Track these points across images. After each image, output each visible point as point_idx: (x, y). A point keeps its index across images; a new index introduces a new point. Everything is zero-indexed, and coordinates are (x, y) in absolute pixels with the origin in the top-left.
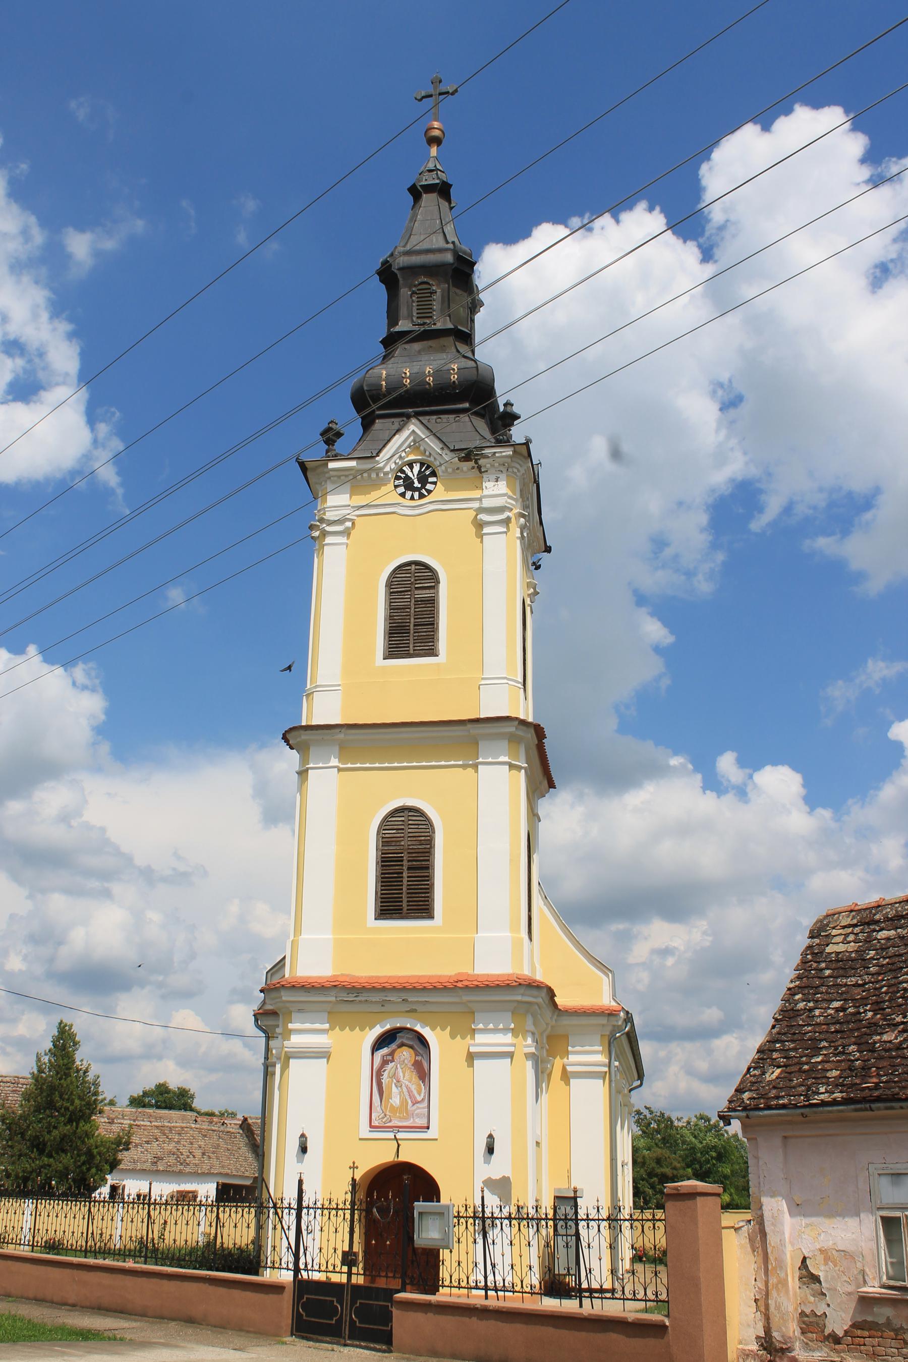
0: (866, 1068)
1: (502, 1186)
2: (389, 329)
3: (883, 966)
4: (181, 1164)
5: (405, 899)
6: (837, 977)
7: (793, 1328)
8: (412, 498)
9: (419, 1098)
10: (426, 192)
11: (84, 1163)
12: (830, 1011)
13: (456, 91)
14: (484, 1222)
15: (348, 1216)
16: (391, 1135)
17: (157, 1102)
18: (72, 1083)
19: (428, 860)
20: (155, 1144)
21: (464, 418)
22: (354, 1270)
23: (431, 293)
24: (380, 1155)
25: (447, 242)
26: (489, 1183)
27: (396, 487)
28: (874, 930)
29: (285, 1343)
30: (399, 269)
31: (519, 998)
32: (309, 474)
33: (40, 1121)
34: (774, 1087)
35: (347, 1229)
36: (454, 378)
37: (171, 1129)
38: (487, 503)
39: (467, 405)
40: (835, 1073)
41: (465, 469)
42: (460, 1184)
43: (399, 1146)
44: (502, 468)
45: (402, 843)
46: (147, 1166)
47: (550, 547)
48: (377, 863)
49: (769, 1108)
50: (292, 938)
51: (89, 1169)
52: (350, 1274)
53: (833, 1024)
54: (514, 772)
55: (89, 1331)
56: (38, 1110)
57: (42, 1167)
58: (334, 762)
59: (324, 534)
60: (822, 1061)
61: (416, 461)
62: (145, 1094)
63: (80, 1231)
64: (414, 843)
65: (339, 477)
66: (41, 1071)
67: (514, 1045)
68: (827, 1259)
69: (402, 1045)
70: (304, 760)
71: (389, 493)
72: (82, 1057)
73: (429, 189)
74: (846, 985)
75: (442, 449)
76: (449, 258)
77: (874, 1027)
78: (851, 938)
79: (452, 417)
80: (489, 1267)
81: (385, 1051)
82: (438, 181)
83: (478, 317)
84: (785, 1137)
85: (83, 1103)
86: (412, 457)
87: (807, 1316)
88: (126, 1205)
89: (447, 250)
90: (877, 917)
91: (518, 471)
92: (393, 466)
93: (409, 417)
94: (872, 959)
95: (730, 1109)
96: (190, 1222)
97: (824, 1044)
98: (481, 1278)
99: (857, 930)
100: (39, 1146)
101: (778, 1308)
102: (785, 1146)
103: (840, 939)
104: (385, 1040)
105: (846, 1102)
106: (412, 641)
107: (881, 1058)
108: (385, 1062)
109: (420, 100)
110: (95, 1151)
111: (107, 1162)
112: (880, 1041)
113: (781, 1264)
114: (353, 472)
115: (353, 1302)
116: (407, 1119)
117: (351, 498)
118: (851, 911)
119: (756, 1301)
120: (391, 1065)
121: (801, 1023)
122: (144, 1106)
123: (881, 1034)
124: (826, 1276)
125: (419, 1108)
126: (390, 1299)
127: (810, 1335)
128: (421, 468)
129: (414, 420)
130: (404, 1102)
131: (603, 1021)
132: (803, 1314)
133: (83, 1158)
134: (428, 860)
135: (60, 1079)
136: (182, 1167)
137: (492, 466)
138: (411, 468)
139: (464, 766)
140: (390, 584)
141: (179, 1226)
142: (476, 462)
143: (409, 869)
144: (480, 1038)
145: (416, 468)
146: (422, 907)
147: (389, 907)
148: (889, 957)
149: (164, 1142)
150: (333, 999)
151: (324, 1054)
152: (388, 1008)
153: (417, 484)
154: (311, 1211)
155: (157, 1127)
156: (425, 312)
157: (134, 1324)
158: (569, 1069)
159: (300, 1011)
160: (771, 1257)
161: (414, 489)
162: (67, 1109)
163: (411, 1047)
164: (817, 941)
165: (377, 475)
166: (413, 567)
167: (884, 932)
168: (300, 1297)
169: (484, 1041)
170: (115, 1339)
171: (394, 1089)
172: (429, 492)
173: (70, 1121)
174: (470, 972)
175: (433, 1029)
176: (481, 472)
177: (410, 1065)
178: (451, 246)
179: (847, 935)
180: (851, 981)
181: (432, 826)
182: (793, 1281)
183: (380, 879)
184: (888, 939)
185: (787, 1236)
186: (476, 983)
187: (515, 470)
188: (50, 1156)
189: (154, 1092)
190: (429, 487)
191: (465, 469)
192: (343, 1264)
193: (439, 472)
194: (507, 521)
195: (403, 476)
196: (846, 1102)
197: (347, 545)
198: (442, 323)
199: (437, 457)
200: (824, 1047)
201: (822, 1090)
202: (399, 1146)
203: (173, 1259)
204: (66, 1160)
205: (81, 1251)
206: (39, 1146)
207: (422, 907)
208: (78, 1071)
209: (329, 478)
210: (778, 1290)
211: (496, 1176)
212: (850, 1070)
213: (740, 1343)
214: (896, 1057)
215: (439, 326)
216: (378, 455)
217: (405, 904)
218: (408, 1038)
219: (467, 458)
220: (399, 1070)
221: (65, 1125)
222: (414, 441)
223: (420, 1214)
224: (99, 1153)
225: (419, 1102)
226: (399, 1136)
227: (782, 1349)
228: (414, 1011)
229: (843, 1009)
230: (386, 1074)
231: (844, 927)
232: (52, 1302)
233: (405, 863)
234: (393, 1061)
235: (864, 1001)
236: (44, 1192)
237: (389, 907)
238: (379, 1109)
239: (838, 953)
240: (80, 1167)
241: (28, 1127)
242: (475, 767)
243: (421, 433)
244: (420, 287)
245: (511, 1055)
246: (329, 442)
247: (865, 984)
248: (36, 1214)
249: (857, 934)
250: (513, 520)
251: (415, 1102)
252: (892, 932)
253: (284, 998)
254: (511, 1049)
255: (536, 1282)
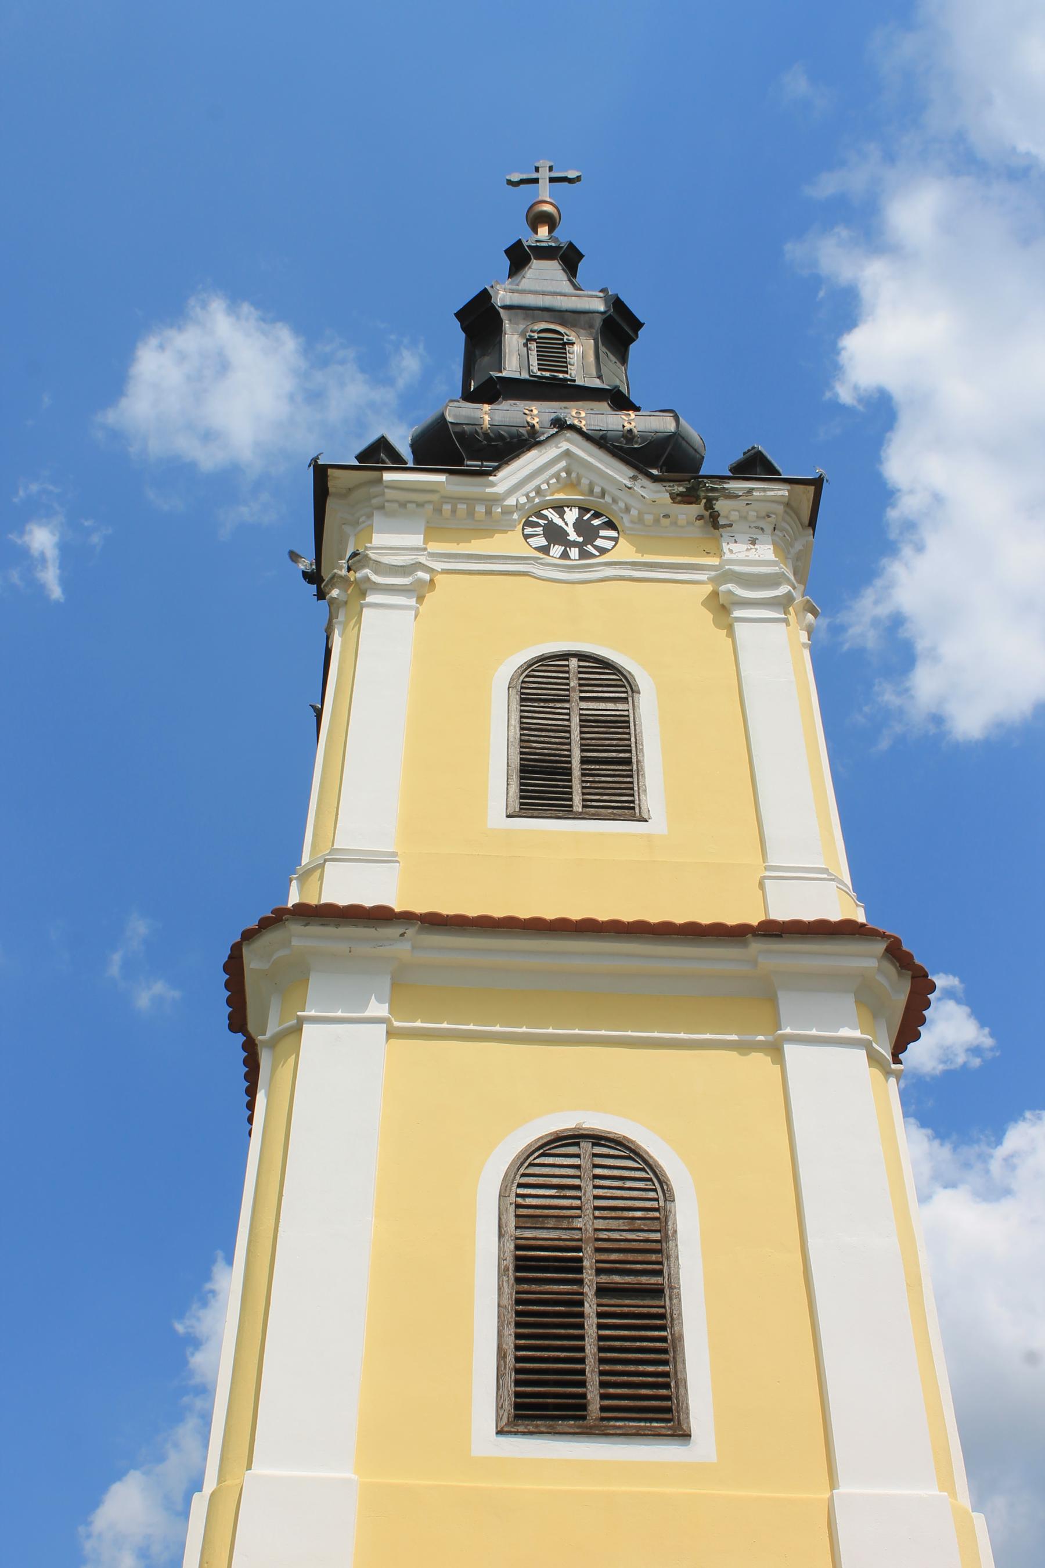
5: (593, 1378)
10: (537, 258)
13: (578, 178)
19: (659, 1273)
23: (565, 344)
32: (331, 504)
41: (682, 519)
44: (761, 524)
45: (578, 1223)
48: (502, 1272)
58: (378, 1009)
64: (613, 1224)
65: (403, 505)
73: (544, 253)
92: (523, 500)
114: (435, 497)
128: (581, 516)
134: (659, 1273)
139: (743, 1047)
142: (709, 506)
145: (572, 515)
146: (648, 1401)
147: (543, 1396)
165: (489, 512)
181: (663, 1182)
183: (511, 1317)
191: (682, 519)
193: (624, 521)
195: (541, 522)
199: (618, 493)
207: (648, 1401)
237: (543, 1396)
242: (775, 1050)
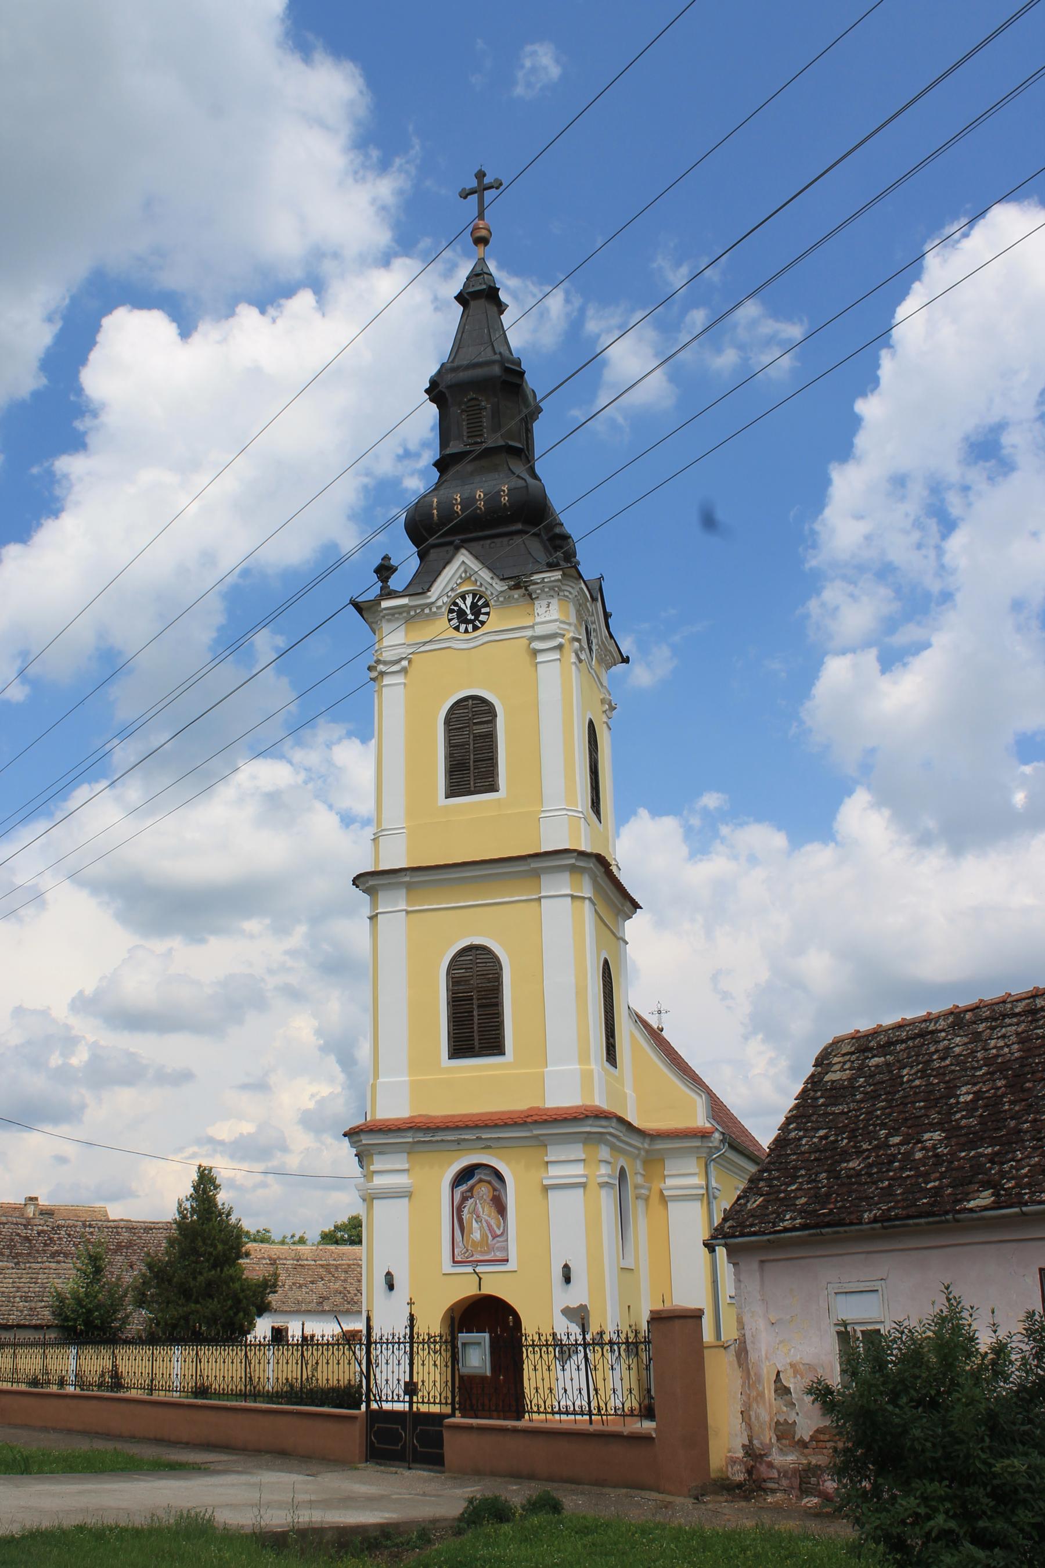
0: (828, 1195)
1: (579, 1315)
2: (441, 451)
3: (867, 1093)
4: (349, 1303)
5: (476, 1037)
6: (827, 1106)
7: (768, 1436)
8: (466, 631)
9: (499, 1232)
11: (231, 1308)
12: (815, 1140)
14: (564, 1350)
15: (408, 1349)
16: (470, 1270)
17: (350, 1236)
18: (213, 1227)
20: (320, 1284)
21: (518, 540)
22: (415, 1399)
24: (465, 1288)
25: (495, 354)
26: (567, 1312)
27: (450, 620)
28: (867, 1058)
29: (356, 1469)
30: (449, 387)
31: (588, 1129)
33: (185, 1267)
34: (752, 1216)
35: (408, 1361)
36: (505, 500)
37: (337, 1267)
38: (539, 631)
39: (519, 526)
40: (803, 1200)
41: (516, 596)
42: (541, 1316)
43: (480, 1279)
44: (552, 593)
46: (313, 1306)
47: (628, 657)
48: (448, 1004)
49: (742, 1235)
50: (371, 1081)
51: (236, 1314)
52: (411, 1403)
53: (815, 1152)
54: (578, 903)
55: (177, 1463)
56: (183, 1255)
57: (190, 1313)
59: (382, 674)
60: (796, 1189)
61: (468, 592)
62: (337, 1228)
63: (576, 1386)
65: (393, 615)
66: (184, 1217)
67: (586, 1176)
68: (796, 1372)
69: (481, 1181)
70: (374, 904)
71: (442, 626)
72: (223, 1198)
74: (833, 1113)
75: (492, 578)
76: (496, 370)
77: (845, 1155)
78: (847, 1066)
79: (505, 540)
80: (592, 1393)
81: (464, 1188)
82: (484, 287)
83: (537, 427)
84: (762, 1262)
85: (227, 1247)
86: (464, 588)
87: (781, 1424)
88: (390, 1346)
89: (493, 362)
90: (872, 1044)
91: (570, 593)
93: (457, 549)
94: (860, 1086)
95: (713, 1237)
96: (330, 1361)
97: (803, 1172)
98: (585, 1403)
99: (854, 1057)
100: (186, 1293)
101: (757, 1417)
102: (762, 1270)
103: (837, 1067)
104: (465, 1175)
105: (804, 1227)
106: (472, 778)
107: (843, 1184)
108: (464, 1199)
109: (465, 198)
110: (241, 1296)
111: (254, 1304)
112: (846, 1168)
113: (759, 1379)
115: (414, 1429)
116: (487, 1253)
117: (406, 635)
118: (853, 1038)
119: (742, 1412)
120: (471, 1201)
121: (789, 1152)
122: (337, 1243)
123: (848, 1161)
124: (795, 1388)
125: (498, 1242)
126: (441, 1425)
127: (784, 1441)
128: (474, 599)
129: (463, 551)
130: (484, 1236)
131: (697, 1143)
132: (778, 1423)
133: (230, 1302)
135: (203, 1224)
136: (349, 1306)
137: (543, 590)
138: (464, 599)
140: (448, 721)
141: (341, 1366)
142: (526, 590)
143: (479, 1007)
144: (554, 1171)
145: (469, 600)
146: (494, 1045)
148: (874, 1085)
149: (330, 1281)
150: (410, 1140)
151: (406, 1194)
152: (463, 1145)
153: (470, 617)
154: (378, 1346)
155: (322, 1266)
156: (475, 430)
157: (234, 1458)
158: (666, 1193)
159: (380, 1153)
160: (752, 1373)
161: (467, 622)
162: (210, 1254)
163: (489, 1182)
164: (819, 1069)
166: (470, 702)
167: (876, 1059)
168: (372, 1426)
169: (557, 1173)
170: (200, 1469)
171: (475, 1224)
172: (483, 623)
173: (214, 1266)
174: (541, 1105)
175: (508, 1164)
176: (532, 599)
177: (488, 1200)
178: (497, 357)
179: (844, 1063)
180: (837, 1110)
182: (769, 1392)
184: (877, 1066)
185: (763, 1353)
186: (545, 1117)
187: (567, 593)
188: (197, 1302)
189: (346, 1226)
190: (482, 618)
192: (405, 1394)
193: (492, 603)
194: (560, 647)
195: (456, 608)
196: (804, 1227)
197: (405, 684)
198: (492, 440)
200: (802, 1175)
201: (788, 1217)
202: (480, 1279)
203: (268, 1396)
204: (213, 1305)
205: (241, 1395)
206: (186, 1293)
207: (494, 1045)
208: (220, 1214)
209: (384, 617)
210: (757, 1402)
211: (574, 1305)
212: (816, 1197)
213: (730, 1451)
214: (853, 1184)
215: (490, 444)
216: (429, 590)
217: (476, 1042)
218: (485, 1174)
219: (517, 587)
220: (479, 1205)
221: (210, 1270)
222: (465, 572)
223: (464, 1344)
224: (246, 1297)
225: (498, 1236)
226: (479, 1269)
227: (761, 1455)
228: (489, 1147)
229: (825, 1137)
230: (466, 1210)
231: (843, 1055)
232: (169, 1441)
233: (475, 1002)
234: (472, 1197)
235: (840, 1131)
236: (197, 1339)
238: (461, 1244)
239: (833, 1082)
240: (226, 1311)
241: (175, 1272)
243: (474, 564)
244: (469, 404)
245: (583, 1185)
246: (384, 580)
247: (850, 1111)
248: (78, 1357)
249: (853, 1062)
250: (567, 646)
251: (495, 1236)
252: (882, 1059)
253: (364, 1142)
254: (584, 1180)
255: (635, 1405)
